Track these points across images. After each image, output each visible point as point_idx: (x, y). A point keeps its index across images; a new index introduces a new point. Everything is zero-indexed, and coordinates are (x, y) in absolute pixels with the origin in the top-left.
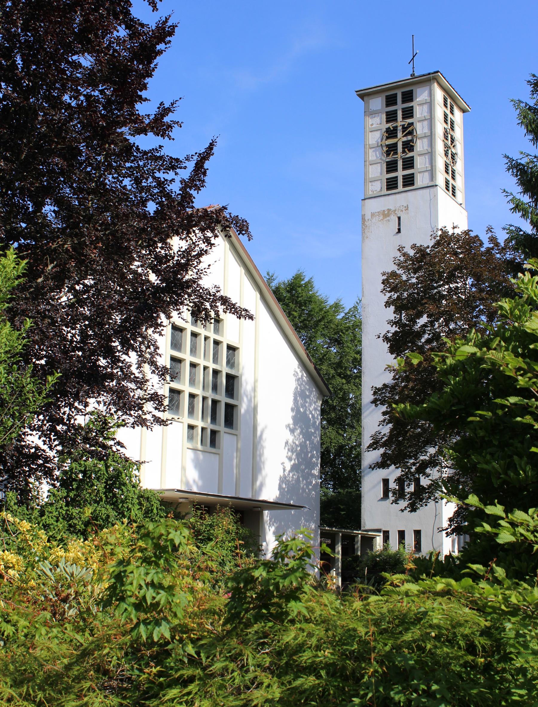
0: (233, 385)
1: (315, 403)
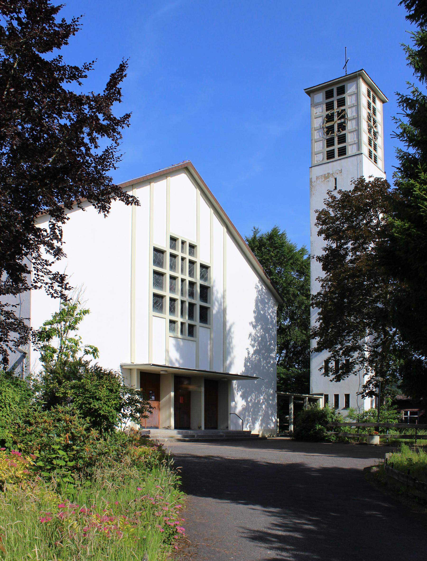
0: (207, 293)
1: (272, 308)
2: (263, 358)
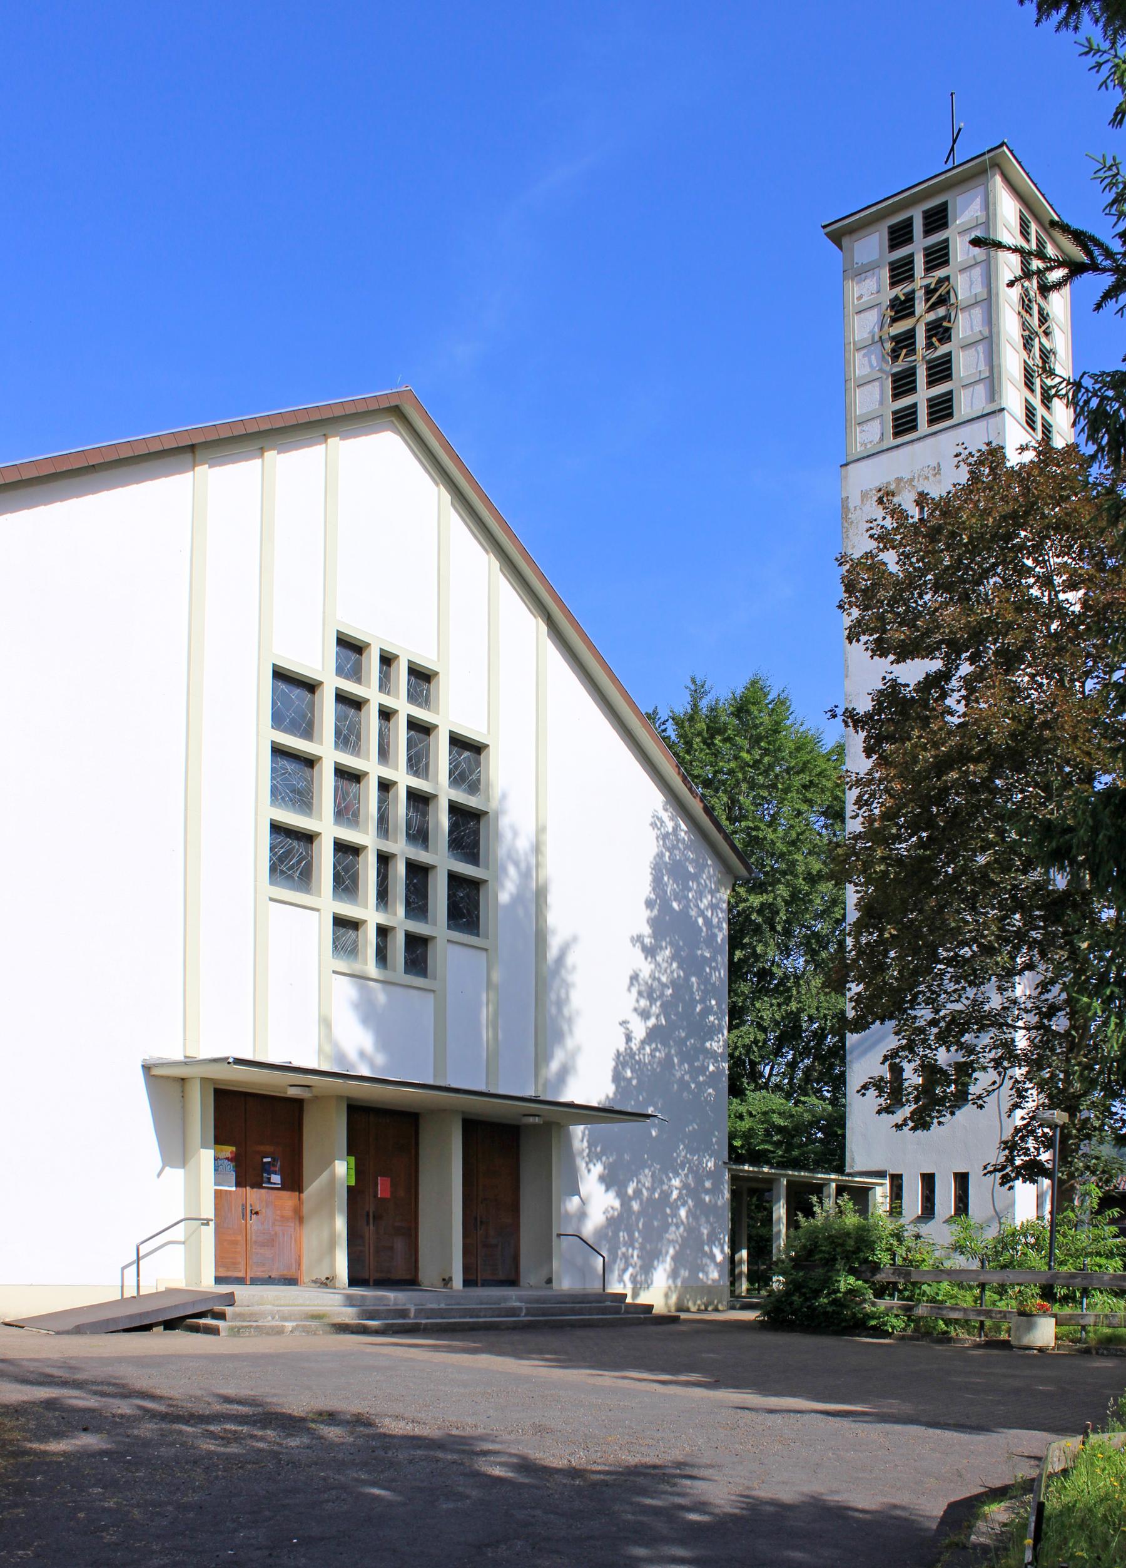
1: (712, 893)
2: (680, 1053)
